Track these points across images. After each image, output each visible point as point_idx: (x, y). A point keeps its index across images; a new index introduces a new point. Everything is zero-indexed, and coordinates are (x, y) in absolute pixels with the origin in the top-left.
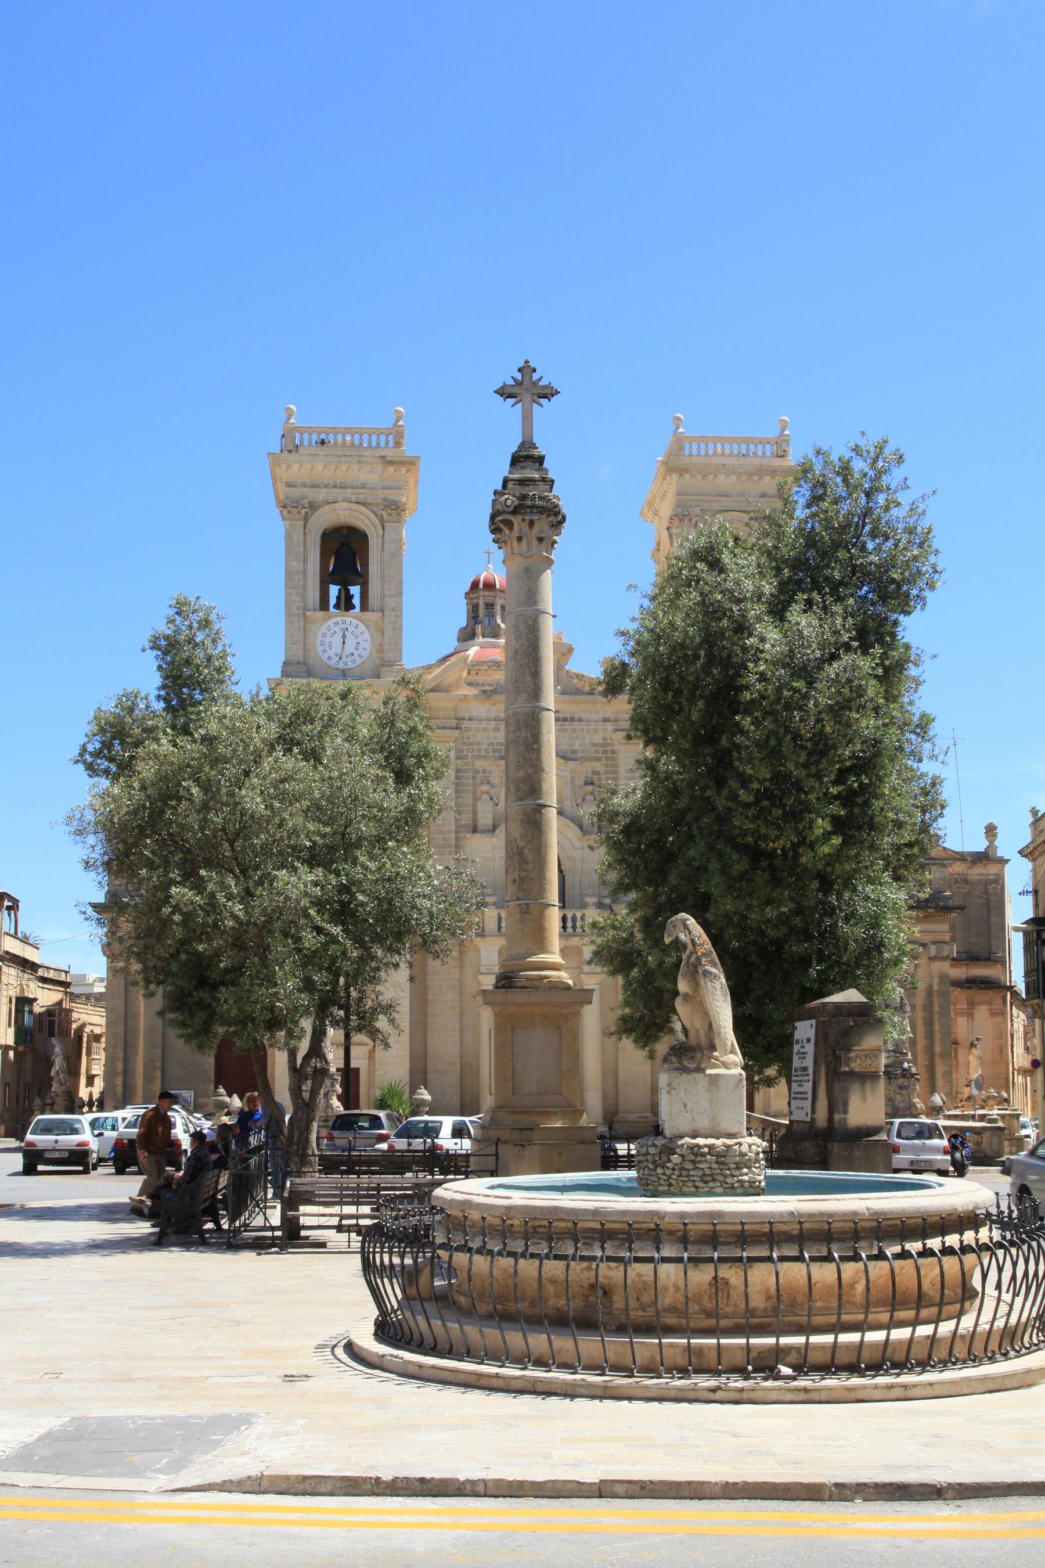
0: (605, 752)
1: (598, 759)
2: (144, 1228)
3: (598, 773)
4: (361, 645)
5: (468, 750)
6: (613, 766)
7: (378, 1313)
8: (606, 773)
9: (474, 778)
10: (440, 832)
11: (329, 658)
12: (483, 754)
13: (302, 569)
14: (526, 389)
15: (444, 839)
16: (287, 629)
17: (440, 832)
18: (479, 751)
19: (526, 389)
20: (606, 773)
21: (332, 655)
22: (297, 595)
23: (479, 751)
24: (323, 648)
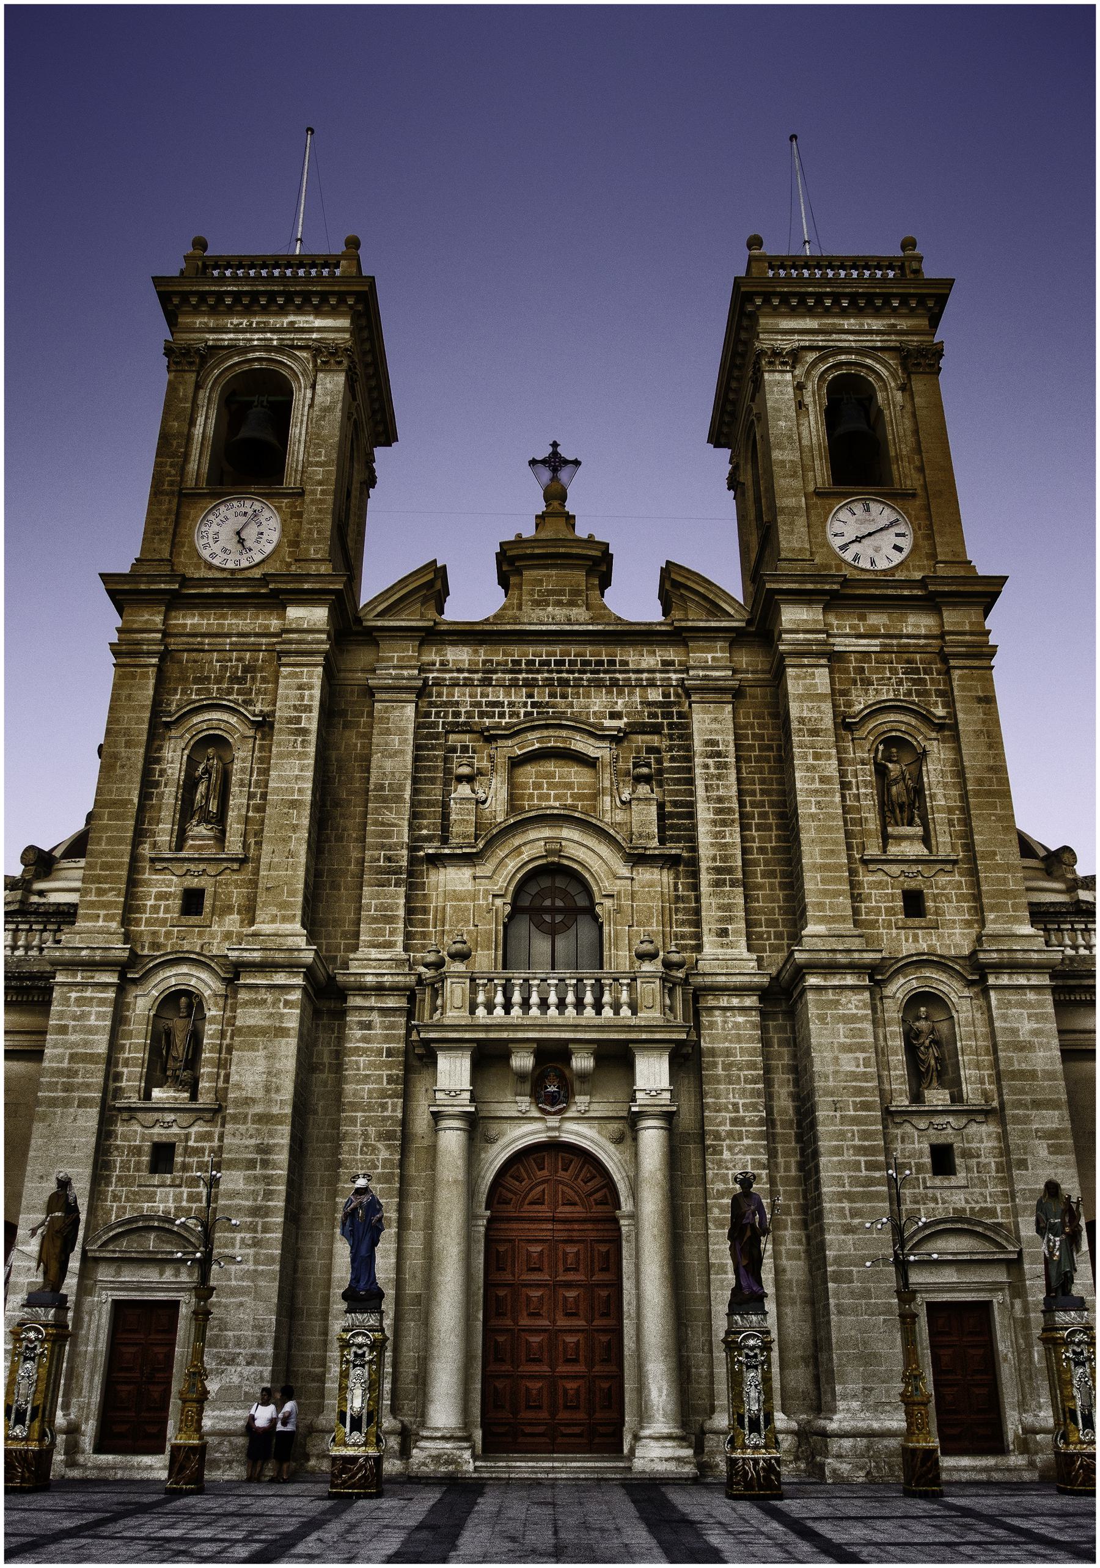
0: (667, 715)
1: (656, 729)
2: (260, 1463)
3: (657, 750)
4: (265, 537)
5: (437, 714)
6: (681, 737)
7: (1053, 849)
8: (671, 748)
9: (446, 760)
10: (383, 846)
11: (213, 555)
12: (462, 720)
13: (186, 431)
14: (555, 462)
15: (388, 859)
16: (150, 512)
17: (383, 846)
18: (457, 714)
19: (555, 462)
20: (671, 748)
21: (218, 552)
22: (171, 466)
23: (457, 714)
24: (205, 541)
